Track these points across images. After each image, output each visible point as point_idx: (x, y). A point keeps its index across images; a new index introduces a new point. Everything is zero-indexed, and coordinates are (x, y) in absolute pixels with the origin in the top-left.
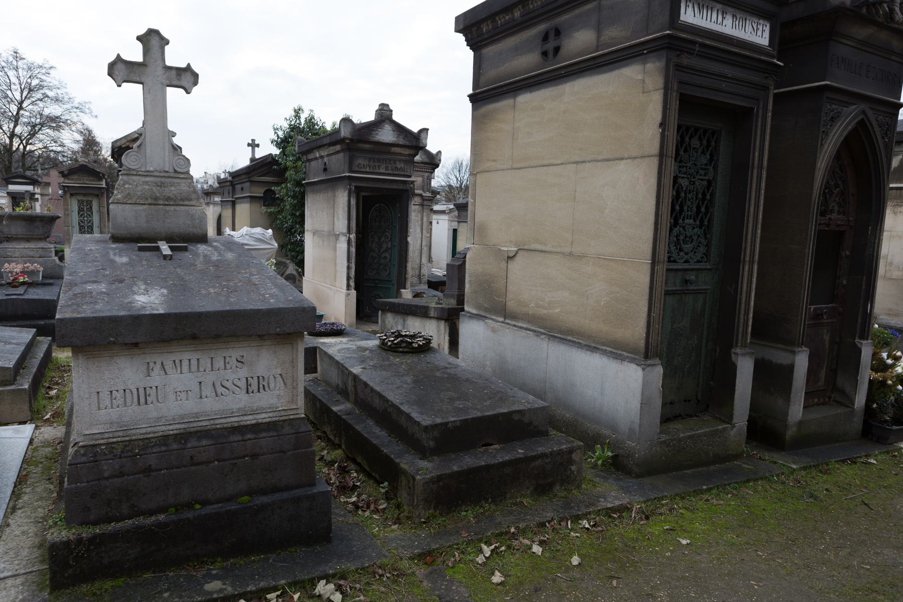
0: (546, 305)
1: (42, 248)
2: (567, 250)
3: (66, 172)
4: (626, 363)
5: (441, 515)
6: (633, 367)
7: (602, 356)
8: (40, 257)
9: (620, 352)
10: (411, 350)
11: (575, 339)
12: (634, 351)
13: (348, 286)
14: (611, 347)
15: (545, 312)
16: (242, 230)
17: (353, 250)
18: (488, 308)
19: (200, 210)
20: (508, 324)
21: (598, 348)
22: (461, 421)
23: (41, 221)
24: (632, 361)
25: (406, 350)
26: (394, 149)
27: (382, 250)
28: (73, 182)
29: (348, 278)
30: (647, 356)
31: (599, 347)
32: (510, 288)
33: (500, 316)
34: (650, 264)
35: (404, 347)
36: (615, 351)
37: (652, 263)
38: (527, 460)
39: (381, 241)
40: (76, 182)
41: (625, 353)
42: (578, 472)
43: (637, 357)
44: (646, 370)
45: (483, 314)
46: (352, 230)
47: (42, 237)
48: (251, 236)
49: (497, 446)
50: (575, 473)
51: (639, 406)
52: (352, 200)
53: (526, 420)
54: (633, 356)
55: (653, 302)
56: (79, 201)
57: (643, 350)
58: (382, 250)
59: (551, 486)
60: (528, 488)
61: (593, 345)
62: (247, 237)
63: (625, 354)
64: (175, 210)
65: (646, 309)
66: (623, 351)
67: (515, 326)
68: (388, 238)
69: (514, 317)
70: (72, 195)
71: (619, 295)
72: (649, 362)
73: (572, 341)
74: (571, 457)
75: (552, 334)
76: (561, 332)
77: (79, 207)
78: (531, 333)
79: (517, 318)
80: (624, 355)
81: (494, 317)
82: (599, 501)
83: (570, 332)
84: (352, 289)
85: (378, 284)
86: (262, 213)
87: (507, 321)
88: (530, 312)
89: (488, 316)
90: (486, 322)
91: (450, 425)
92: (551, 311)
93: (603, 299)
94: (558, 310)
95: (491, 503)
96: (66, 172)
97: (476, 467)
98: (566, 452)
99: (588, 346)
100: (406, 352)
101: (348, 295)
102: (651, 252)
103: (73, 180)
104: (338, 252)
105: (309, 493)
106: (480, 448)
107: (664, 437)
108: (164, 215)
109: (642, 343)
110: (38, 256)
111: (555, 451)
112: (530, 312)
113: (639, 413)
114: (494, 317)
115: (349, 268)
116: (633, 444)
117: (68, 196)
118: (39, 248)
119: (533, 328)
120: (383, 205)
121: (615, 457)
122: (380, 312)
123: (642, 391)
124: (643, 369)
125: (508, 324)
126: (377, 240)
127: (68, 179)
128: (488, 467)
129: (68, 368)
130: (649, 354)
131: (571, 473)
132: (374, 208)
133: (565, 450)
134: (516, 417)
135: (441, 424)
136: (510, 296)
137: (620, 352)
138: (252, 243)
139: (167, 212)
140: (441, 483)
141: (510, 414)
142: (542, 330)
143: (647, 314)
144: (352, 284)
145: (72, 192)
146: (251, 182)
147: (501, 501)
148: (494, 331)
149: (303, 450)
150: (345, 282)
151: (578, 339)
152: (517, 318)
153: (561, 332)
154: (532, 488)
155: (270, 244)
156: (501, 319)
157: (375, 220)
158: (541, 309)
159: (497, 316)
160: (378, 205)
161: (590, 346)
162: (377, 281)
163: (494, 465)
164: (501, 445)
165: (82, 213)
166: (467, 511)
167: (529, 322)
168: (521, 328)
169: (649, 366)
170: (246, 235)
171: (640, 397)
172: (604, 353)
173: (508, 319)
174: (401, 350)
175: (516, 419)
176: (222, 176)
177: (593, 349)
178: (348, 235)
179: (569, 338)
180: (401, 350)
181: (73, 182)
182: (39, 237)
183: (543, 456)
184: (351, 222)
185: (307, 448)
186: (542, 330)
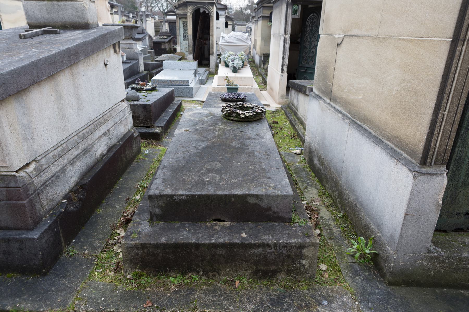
1: (129, 43)
2: (375, 33)
3: (177, 6)
4: (400, 164)
5: (149, 275)
6: (405, 171)
7: (382, 150)
8: (128, 48)
9: (399, 151)
10: (239, 119)
11: (368, 128)
12: (411, 153)
13: (282, 70)
14: (393, 143)
16: (230, 33)
17: (288, 46)
19: (81, 4)
20: (331, 105)
21: (383, 142)
22: (187, 196)
23: (128, 28)
24: (407, 164)
25: (236, 119)
27: (312, 47)
28: (180, 11)
29: (283, 65)
30: (424, 161)
31: (383, 140)
34: (450, 43)
35: (234, 117)
36: (395, 148)
37: (452, 41)
38: (245, 246)
39: (312, 41)
40: (182, 11)
41: (403, 153)
42: (310, 266)
43: (414, 161)
44: (419, 178)
45: (320, 95)
46: (288, 32)
47: (129, 37)
48: (234, 37)
49: (227, 224)
50: (306, 267)
51: (403, 216)
52: (288, 10)
53: (264, 204)
54: (410, 158)
55: (445, 96)
56: (183, 22)
57: (420, 154)
58: (312, 47)
59: (274, 273)
60: (246, 270)
61: (380, 137)
62: (233, 38)
63: (404, 155)
64: (64, 5)
65: (433, 105)
66: (402, 150)
68: (316, 39)
70: (180, 18)
71: (409, 84)
72: (425, 170)
73: (366, 131)
74: (301, 252)
75: (354, 120)
76: (360, 119)
77: (183, 25)
79: (336, 101)
80: (402, 155)
81: (325, 99)
82: (320, 304)
83: (365, 120)
84: (285, 72)
85: (307, 70)
86: (268, 26)
87: (332, 103)
88: (344, 97)
89: (323, 97)
91: (176, 197)
93: (395, 89)
95: (202, 275)
96: (177, 6)
97: (183, 243)
98: (295, 246)
99: (376, 137)
100: (236, 121)
101: (282, 76)
102: (454, 26)
103: (180, 10)
104: (280, 47)
105: (17, 237)
106: (209, 222)
107: (439, 252)
108: (58, 8)
109: (421, 146)
110: (127, 48)
111: (280, 244)
112: (344, 97)
113: (401, 224)
114: (325, 99)
115: (283, 58)
116: (392, 252)
117: (178, 19)
118: (128, 43)
119: (344, 112)
120: (315, 14)
121: (375, 256)
122: (290, 88)
123: (409, 202)
124: (414, 177)
125: (331, 105)
126: (309, 40)
127: (178, 10)
128: (197, 246)
130: (428, 161)
131: (301, 266)
132: (309, 17)
133: (294, 245)
134: (252, 201)
135: (167, 196)
137: (399, 151)
138: (235, 41)
139: (59, 6)
140: (146, 250)
141: (244, 197)
142: (348, 115)
143: (432, 111)
144: (286, 69)
145: (180, 17)
146: (263, 7)
147: (214, 276)
149: (15, 202)
150: (281, 67)
151: (370, 128)
152: (336, 101)
153: (360, 119)
154: (251, 271)
155: (246, 43)
156: (328, 101)
157: (309, 25)
160: (312, 15)
161: (378, 138)
162: (306, 68)
163: (204, 245)
164: (233, 224)
165: (184, 28)
166: (176, 278)
167: (343, 106)
168: (337, 110)
169: (424, 174)
170: (232, 36)
171: (406, 207)
172: (386, 148)
174: (232, 118)
175: (252, 202)
177: (377, 141)
178: (284, 35)
179: (364, 126)
180: (232, 118)
181: (180, 11)
182: (128, 37)
183: (265, 245)
184: (287, 26)
185: (19, 201)
186: (348, 115)
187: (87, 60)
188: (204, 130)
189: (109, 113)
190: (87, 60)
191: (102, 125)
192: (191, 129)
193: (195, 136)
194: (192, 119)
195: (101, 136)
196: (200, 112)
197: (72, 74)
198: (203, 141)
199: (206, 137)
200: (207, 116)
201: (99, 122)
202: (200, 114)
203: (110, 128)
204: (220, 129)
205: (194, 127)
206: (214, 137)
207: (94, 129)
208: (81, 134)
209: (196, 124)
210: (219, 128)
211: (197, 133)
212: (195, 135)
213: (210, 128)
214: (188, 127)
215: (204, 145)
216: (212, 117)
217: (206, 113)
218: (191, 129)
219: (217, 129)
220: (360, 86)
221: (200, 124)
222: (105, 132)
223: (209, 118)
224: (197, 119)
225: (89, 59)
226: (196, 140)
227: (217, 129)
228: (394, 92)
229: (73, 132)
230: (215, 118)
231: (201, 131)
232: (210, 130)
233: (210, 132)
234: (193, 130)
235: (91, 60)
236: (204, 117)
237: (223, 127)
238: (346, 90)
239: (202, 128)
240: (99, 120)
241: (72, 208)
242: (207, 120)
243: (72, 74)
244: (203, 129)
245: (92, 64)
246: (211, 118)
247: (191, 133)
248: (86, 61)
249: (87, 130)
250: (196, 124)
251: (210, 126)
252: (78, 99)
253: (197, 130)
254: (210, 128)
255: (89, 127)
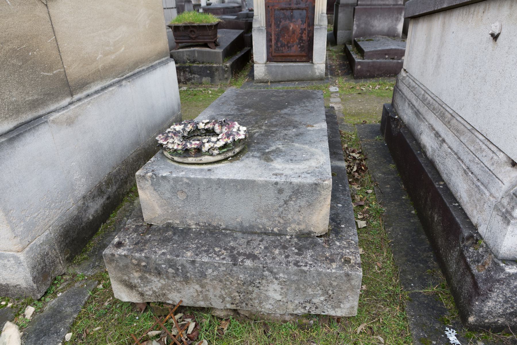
0: (112, 48)
15: (113, 57)
18: (37, 100)
20: (80, 100)
26: (477, 134)
32: (64, 46)
33: (63, 98)
67: (88, 96)
69: (83, 85)
75: (125, 77)
78: (113, 88)
81: (52, 107)
87: (76, 97)
89: (41, 112)
90: (53, 122)
92: (117, 53)
94: (123, 49)
114: (52, 107)
129: (270, 7)
136: (67, 59)
148: (70, 122)
153: (130, 69)
158: (109, 56)
159: (58, 101)
167: (102, 78)
168: (97, 92)
173: (77, 93)
176: (261, 33)
179: (137, 70)
187: (465, 13)
188: (284, 126)
189: (462, 127)
190: (465, 13)
191: (441, 118)
192: (304, 128)
193: (297, 119)
194: (307, 147)
195: (434, 130)
196: (292, 166)
197: (444, 23)
198: (285, 114)
199: (282, 117)
200: (278, 152)
201: (444, 114)
202: (292, 157)
203: (446, 143)
204: (260, 127)
205: (301, 131)
206: (272, 117)
207: (434, 109)
208: (427, 96)
209: (297, 135)
210: (260, 128)
211: (294, 123)
212: (296, 120)
213: (274, 129)
214: (309, 130)
215: (285, 111)
216: (267, 151)
217: (279, 160)
218: (304, 128)
219: (264, 127)
220: (117, 39)
221: (291, 136)
222: (440, 136)
223: (273, 148)
224: (297, 145)
225: (469, 12)
226: (295, 115)
227: (264, 127)
228: (147, 26)
229: (425, 85)
230: (262, 146)
231: (289, 125)
232: (276, 126)
233: (275, 123)
234: (301, 126)
235: (471, 16)
236: (283, 149)
237: (254, 130)
238: (100, 56)
239: (287, 128)
240: (447, 113)
241: (393, 126)
242: (277, 142)
243: (444, 23)
244: (285, 127)
245: (470, 21)
246: (269, 146)
247: (303, 123)
248: (463, 14)
249: (432, 100)
250: (297, 135)
251: (273, 132)
252: (439, 56)
253: (295, 127)
254: (274, 129)
255: (434, 102)
